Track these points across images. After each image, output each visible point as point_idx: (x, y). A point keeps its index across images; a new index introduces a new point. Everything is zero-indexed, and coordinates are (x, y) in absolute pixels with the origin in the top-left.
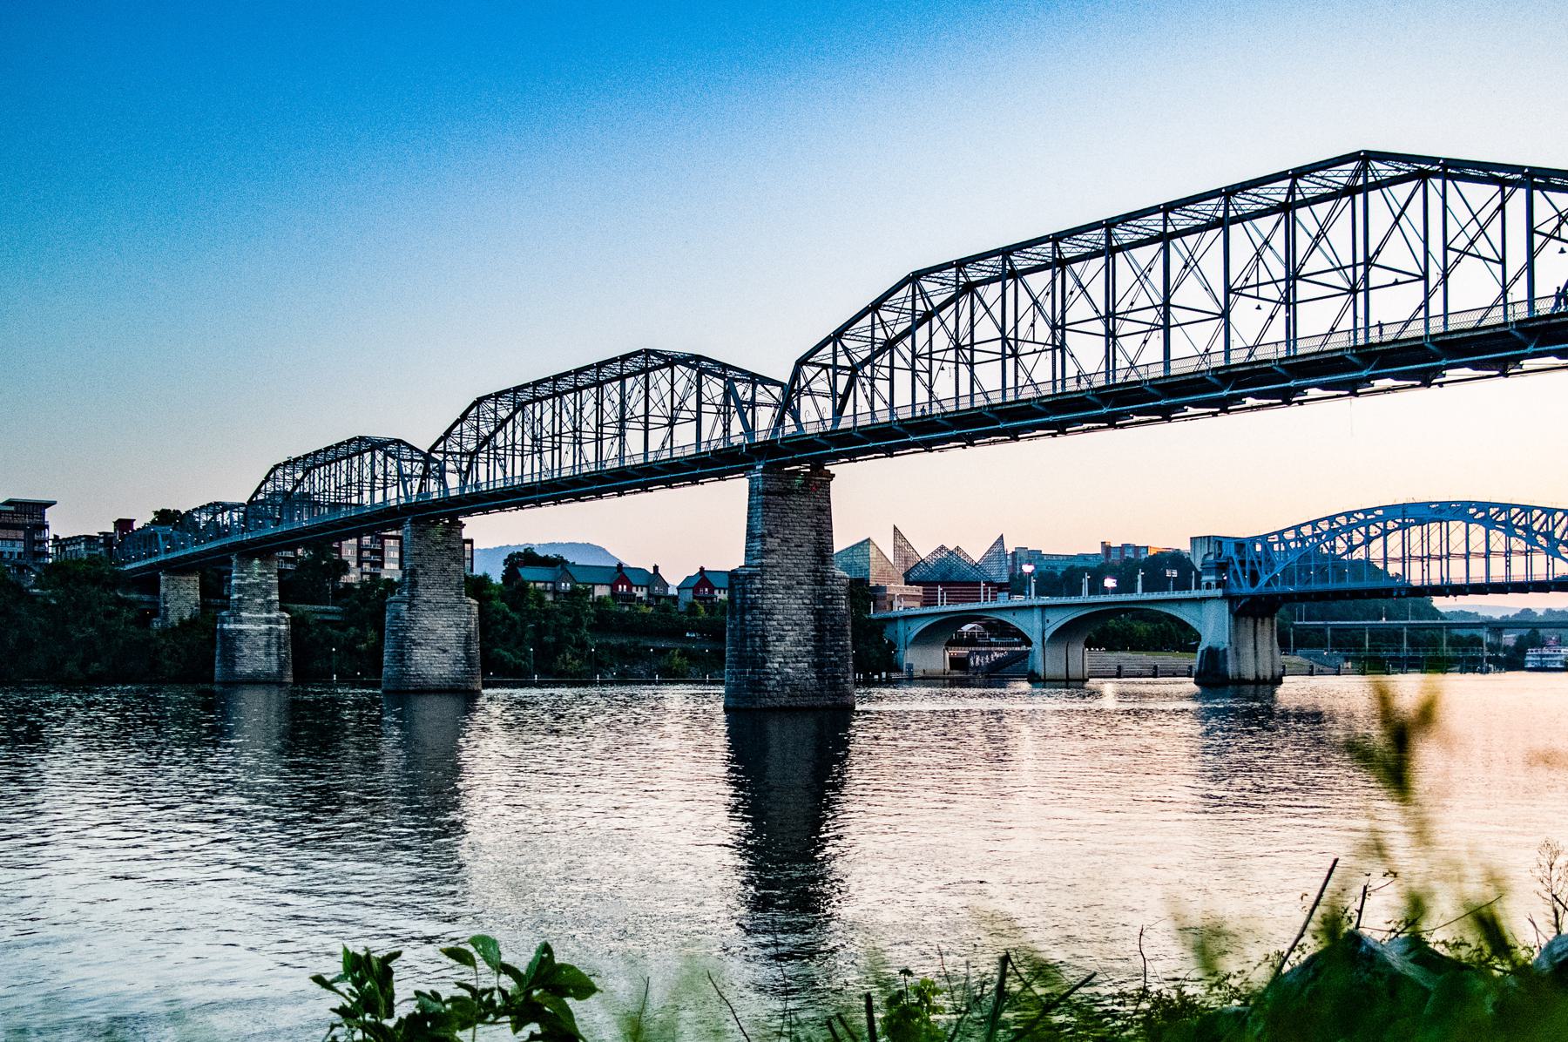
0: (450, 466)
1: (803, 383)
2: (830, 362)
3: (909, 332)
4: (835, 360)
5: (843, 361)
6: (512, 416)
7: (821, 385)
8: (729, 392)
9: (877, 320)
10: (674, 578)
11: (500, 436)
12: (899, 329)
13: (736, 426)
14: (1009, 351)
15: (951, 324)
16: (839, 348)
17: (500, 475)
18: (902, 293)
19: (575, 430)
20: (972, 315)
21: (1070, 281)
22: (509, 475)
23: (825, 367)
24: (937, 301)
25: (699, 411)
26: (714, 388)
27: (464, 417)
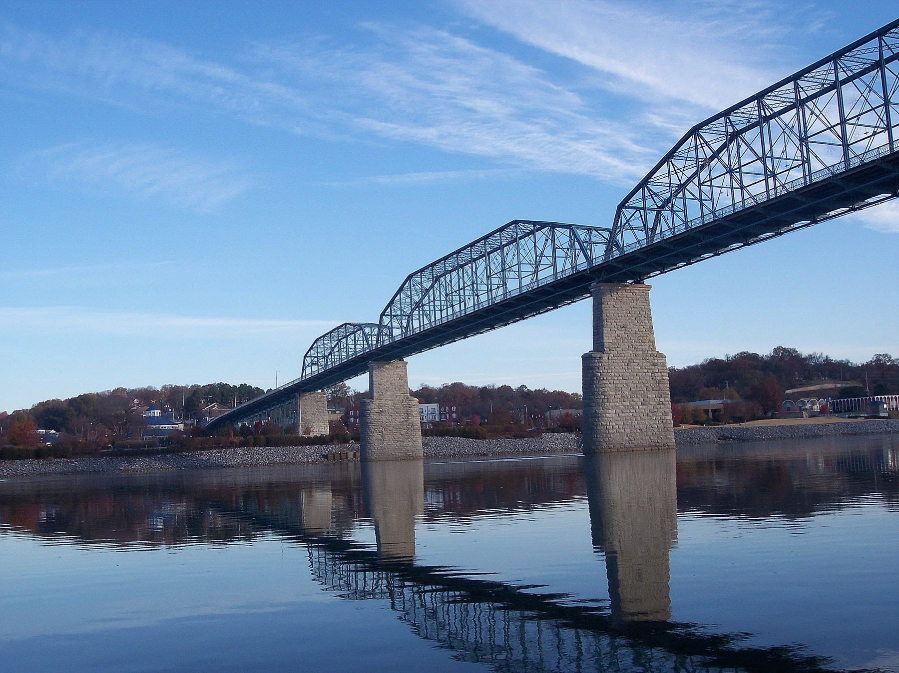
0: (395, 324)
1: (624, 221)
2: (641, 205)
3: (696, 174)
4: (644, 203)
5: (650, 203)
6: (432, 287)
7: (637, 223)
8: (574, 237)
9: (672, 169)
10: (265, 391)
11: (426, 301)
12: (689, 173)
13: (582, 259)
14: (735, 185)
15: (726, 160)
16: (647, 193)
17: (426, 322)
18: (751, 105)
19: (473, 283)
20: (738, 152)
21: (808, 113)
22: (433, 320)
23: (638, 209)
24: (716, 147)
25: (555, 258)
26: (562, 237)
27: (401, 289)
